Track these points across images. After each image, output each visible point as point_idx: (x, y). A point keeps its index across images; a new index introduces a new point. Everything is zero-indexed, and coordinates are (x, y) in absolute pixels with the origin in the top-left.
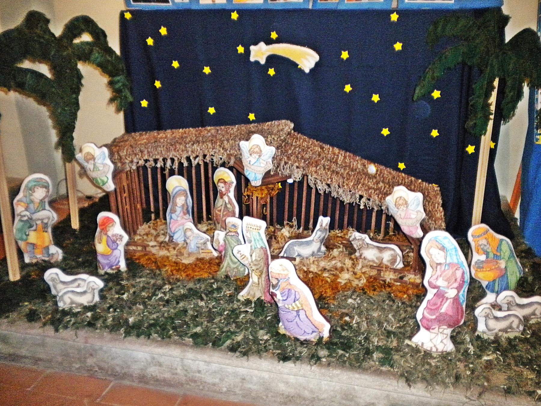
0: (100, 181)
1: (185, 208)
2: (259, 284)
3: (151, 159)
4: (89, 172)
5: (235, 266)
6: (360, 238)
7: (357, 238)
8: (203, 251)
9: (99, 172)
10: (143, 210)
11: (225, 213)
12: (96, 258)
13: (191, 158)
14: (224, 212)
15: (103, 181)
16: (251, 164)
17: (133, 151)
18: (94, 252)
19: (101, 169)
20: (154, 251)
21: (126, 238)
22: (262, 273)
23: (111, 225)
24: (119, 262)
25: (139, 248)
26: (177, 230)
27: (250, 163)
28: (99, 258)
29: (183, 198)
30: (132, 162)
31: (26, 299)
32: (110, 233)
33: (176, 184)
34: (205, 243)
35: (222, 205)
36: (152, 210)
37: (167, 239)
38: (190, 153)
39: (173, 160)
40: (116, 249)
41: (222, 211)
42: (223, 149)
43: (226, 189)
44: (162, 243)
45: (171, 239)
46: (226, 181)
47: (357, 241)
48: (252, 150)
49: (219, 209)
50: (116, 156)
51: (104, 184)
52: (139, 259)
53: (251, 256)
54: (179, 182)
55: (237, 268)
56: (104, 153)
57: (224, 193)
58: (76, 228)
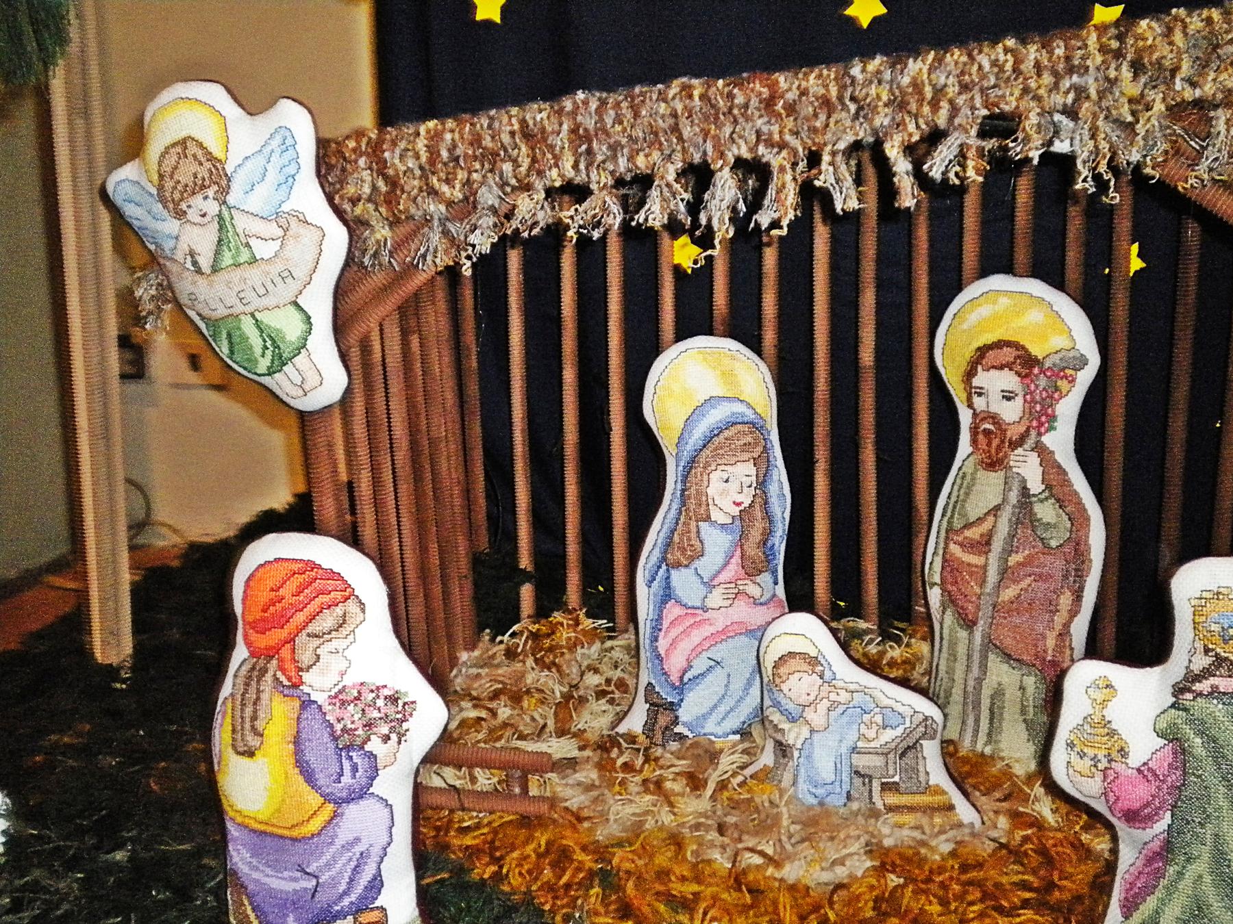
0: (256, 341)
1: (755, 535)
3: (599, 179)
4: (186, 285)
8: (892, 799)
9: (254, 275)
10: (477, 561)
11: (1014, 559)
12: (220, 846)
13: (893, 150)
14: (1008, 551)
15: (272, 340)
17: (476, 141)
18: (208, 803)
19: (263, 250)
20: (570, 792)
21: (430, 715)
23: (327, 621)
24: (376, 884)
25: (485, 780)
26: (700, 665)
28: (240, 857)
29: (745, 471)
30: (467, 207)
31: (1037, 39)
32: (318, 684)
33: (705, 386)
36: (525, 562)
37: (635, 722)
38: (882, 119)
39: (755, 172)
40: (360, 794)
41: (997, 545)
42: (1137, 67)
43: (1030, 403)
44: (607, 744)
45: (663, 720)
46: (1036, 350)
48: (169, 184)
49: (974, 533)
50: (363, 181)
51: (280, 362)
52: (492, 851)
54: (728, 376)
56: (288, 144)
58: (114, 660)
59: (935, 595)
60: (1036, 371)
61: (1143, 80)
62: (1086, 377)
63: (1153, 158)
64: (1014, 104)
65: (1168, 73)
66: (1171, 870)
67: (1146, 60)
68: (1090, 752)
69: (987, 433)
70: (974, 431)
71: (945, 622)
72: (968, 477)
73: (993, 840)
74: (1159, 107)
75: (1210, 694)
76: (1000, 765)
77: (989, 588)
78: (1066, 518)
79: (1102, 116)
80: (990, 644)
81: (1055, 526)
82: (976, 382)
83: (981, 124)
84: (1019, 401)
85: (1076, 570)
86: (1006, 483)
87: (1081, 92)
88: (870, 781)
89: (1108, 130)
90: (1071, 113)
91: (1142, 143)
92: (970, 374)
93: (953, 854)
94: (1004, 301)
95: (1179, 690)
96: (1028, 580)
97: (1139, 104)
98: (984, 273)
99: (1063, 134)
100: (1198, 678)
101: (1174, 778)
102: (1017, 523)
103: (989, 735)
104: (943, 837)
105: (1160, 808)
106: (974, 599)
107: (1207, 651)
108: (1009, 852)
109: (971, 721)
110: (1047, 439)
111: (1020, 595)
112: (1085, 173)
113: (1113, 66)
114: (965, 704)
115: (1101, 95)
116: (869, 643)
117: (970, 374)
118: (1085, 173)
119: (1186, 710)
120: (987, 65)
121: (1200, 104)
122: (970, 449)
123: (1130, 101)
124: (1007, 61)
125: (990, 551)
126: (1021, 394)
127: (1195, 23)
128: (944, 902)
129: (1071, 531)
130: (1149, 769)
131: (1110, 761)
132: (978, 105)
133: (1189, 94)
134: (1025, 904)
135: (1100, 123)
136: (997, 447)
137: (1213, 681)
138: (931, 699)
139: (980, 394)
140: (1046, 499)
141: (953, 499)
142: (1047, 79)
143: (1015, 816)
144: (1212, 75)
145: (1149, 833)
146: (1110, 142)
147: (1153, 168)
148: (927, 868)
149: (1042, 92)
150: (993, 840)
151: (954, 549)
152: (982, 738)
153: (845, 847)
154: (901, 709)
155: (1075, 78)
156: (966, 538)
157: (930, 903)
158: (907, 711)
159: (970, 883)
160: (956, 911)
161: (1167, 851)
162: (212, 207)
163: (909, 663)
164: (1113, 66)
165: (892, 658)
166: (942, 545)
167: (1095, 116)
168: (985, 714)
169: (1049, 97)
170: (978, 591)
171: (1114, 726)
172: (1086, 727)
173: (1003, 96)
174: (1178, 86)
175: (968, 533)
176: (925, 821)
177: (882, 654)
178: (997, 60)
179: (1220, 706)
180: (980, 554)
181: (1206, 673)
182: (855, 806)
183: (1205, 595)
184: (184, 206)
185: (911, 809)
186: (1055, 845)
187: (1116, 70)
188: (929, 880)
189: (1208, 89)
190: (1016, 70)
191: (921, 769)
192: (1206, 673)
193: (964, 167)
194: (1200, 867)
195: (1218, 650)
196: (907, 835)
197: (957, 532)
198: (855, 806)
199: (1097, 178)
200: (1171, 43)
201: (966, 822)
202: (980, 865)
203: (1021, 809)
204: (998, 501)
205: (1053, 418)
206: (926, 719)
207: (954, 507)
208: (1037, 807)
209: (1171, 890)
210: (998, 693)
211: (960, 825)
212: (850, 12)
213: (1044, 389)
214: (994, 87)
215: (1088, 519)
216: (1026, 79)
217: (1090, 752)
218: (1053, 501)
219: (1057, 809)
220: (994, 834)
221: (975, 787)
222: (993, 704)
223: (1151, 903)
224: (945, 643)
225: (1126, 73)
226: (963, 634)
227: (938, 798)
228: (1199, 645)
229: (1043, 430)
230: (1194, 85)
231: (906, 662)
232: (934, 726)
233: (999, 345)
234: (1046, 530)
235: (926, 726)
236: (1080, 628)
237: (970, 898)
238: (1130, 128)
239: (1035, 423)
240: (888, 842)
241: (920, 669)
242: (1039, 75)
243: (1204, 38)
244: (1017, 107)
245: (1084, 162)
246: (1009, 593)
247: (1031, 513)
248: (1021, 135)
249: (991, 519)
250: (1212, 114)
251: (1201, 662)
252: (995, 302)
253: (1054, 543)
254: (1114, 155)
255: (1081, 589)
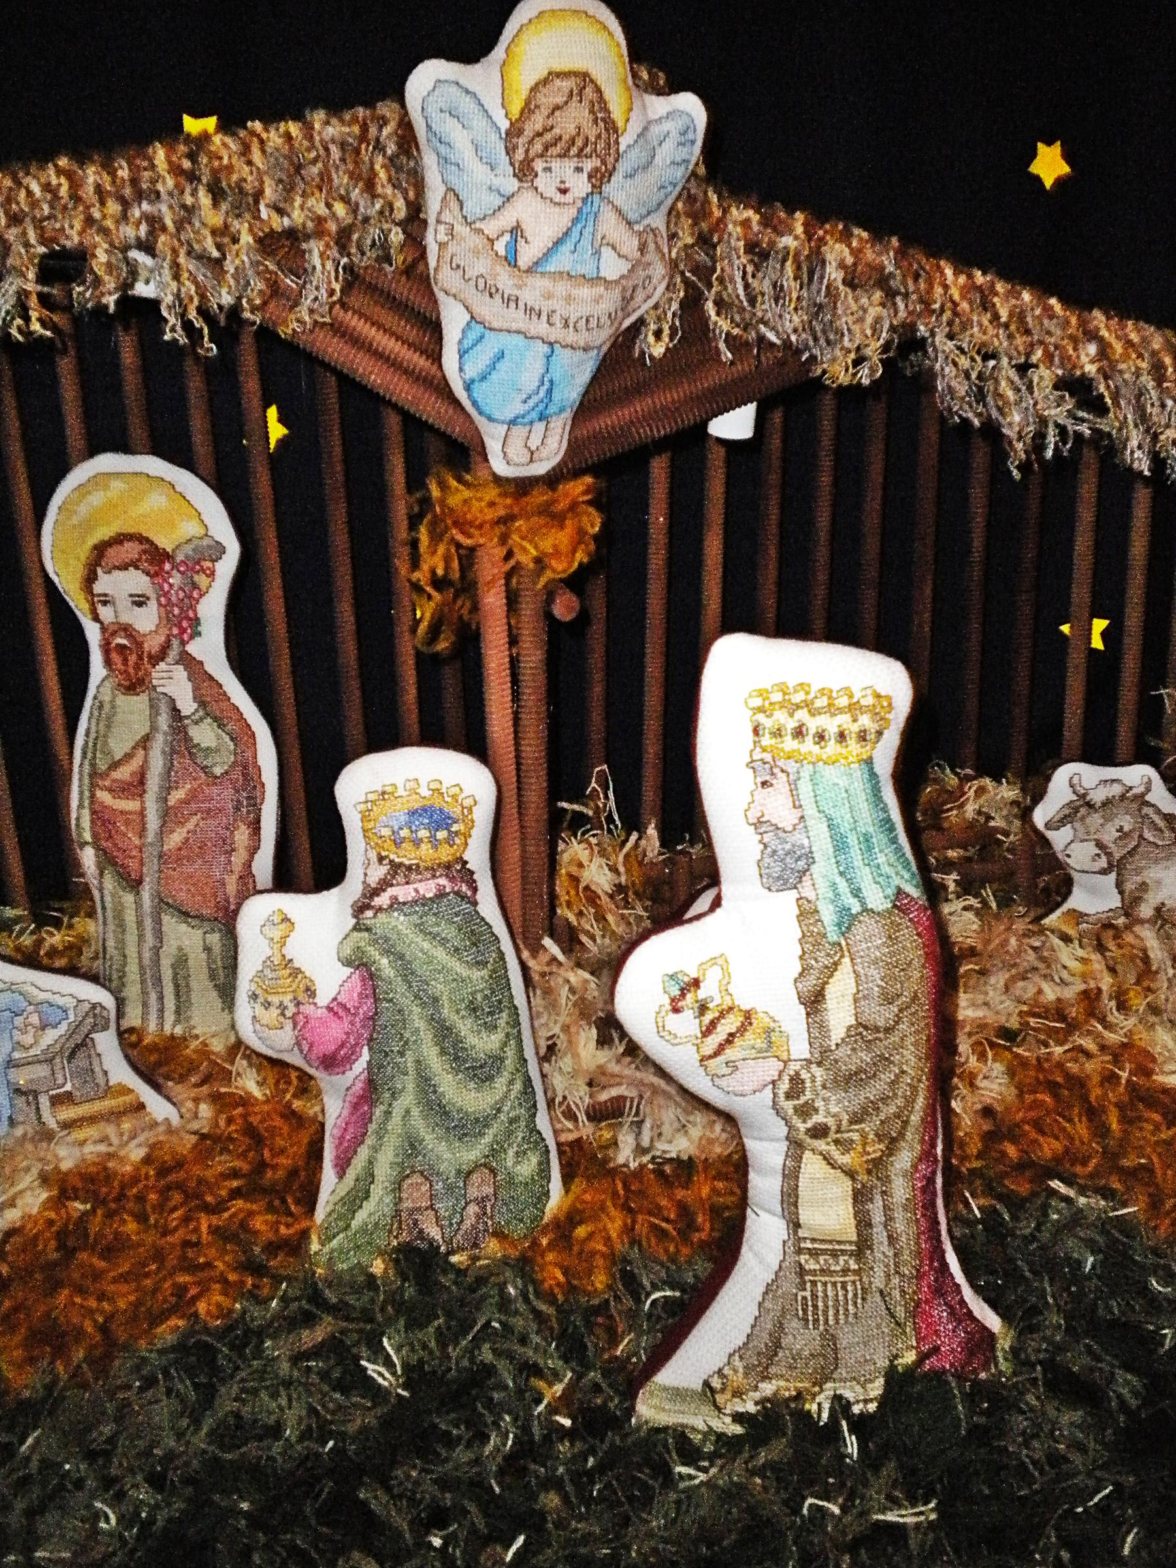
2: (863, 1246)
5: (472, 1154)
6: (1117, 790)
7: (1098, 796)
8: (68, 1113)
14: (168, 788)
16: (527, 255)
22: (892, 1144)
27: (511, 260)
34: (79, 1047)
35: (145, 742)
42: (217, 194)
43: (166, 606)
46: (165, 542)
47: (1096, 819)
48: (537, 122)
49: (124, 773)
53: (814, 1002)
55: (488, 1165)
57: (152, 645)
59: (88, 858)
60: (167, 567)
61: (224, 207)
62: (227, 567)
63: (250, 301)
64: (76, 239)
65: (251, 200)
66: (378, 1112)
67: (224, 184)
68: (275, 1000)
69: (121, 647)
70: (106, 648)
71: (105, 887)
72: (107, 707)
73: (195, 1133)
74: (246, 239)
75: (391, 906)
76: (194, 1044)
77: (151, 837)
78: (227, 738)
79: (182, 252)
80: (162, 903)
81: (217, 750)
82: (98, 588)
83: (40, 263)
84: (153, 605)
85: (248, 798)
86: (151, 707)
87: (155, 224)
88: (36, 1098)
89: (191, 267)
90: (148, 247)
91: (232, 282)
92: (90, 579)
93: (147, 1160)
94: (117, 485)
95: (359, 909)
96: (194, 820)
97: (224, 234)
98: (92, 452)
99: (144, 274)
100: (376, 892)
101: (367, 1006)
102: (171, 753)
103: (178, 1012)
104: (135, 1142)
105: (357, 1044)
106: (134, 853)
107: (381, 859)
108: (209, 1142)
109: (153, 997)
110: (192, 648)
111: (187, 839)
112: (172, 320)
113: (188, 190)
114: (143, 982)
115: (180, 225)
116: (22, 932)
117: (90, 579)
118: (172, 320)
119: (368, 930)
120: (35, 188)
121: (293, 235)
122: (104, 672)
123: (214, 233)
124: (60, 185)
125: (145, 791)
126: (153, 596)
127: (274, 138)
128: (142, 1218)
129: (235, 754)
130: (340, 1004)
131: (298, 1004)
132: (33, 241)
133: (279, 223)
134: (236, 1194)
135: (182, 260)
136: (134, 666)
137: (390, 891)
138: (104, 986)
139: (105, 603)
140: (201, 719)
141: (93, 735)
142: (113, 207)
143: (216, 1098)
144: (298, 201)
145: (350, 1075)
146: (195, 282)
147: (252, 312)
148: (116, 1184)
149: (109, 223)
150: (195, 1133)
151: (104, 796)
152: (170, 1017)
153: (12, 1185)
154: (60, 1001)
155: (145, 206)
156: (114, 781)
157: (125, 1221)
158: (70, 1003)
159: (169, 1188)
160: (155, 1226)
161: (371, 1091)
162: (580, 186)
163: (74, 949)
164: (188, 190)
165: (52, 946)
166: (87, 794)
167: (175, 252)
168: (169, 990)
169: (118, 229)
170: (137, 842)
171: (296, 964)
172: (267, 972)
173: (63, 229)
174: (264, 214)
175: (117, 775)
176: (110, 1130)
177: (39, 943)
178: (49, 184)
179: (402, 918)
180: (133, 797)
181: (384, 884)
182: (19, 1132)
183: (371, 797)
184: (539, 165)
185: (92, 1120)
186: (261, 1122)
187: (192, 195)
188: (121, 1196)
189: (298, 217)
190: (76, 198)
191: (97, 1069)
192: (384, 884)
193: (27, 319)
194: (408, 1100)
195: (392, 857)
196: (92, 1150)
197: (105, 775)
198: (19, 1132)
199: (188, 326)
200: (250, 163)
201: (160, 1119)
202: (180, 1164)
203: (223, 1090)
204: (147, 730)
205: (196, 621)
206: (94, 1006)
207: (95, 745)
208: (240, 1083)
209: (380, 1134)
210: (181, 962)
211: (154, 1124)
212: (1048, 183)
213: (181, 588)
214: (48, 218)
215: (253, 735)
216: (88, 208)
217: (275, 1000)
218: (209, 720)
219: (265, 1079)
220: (195, 1126)
221: (168, 1078)
222: (175, 975)
223: (363, 1153)
224: (109, 914)
225: (205, 199)
226: (129, 898)
227: (127, 1099)
228: (373, 855)
229: (186, 637)
230: (281, 212)
231: (70, 947)
232: (105, 1013)
233: (120, 539)
234: (206, 757)
235: (95, 1016)
236: (264, 864)
237: (173, 1203)
238: (217, 265)
239: (175, 631)
240: (65, 1166)
241: (88, 953)
242: (103, 203)
243: (285, 157)
244: (81, 243)
245: (169, 307)
246: (176, 838)
247: (187, 739)
248: (89, 278)
249: (141, 753)
250: (304, 246)
251: (378, 873)
252: (106, 487)
253: (218, 771)
254: (203, 296)
255: (258, 821)
